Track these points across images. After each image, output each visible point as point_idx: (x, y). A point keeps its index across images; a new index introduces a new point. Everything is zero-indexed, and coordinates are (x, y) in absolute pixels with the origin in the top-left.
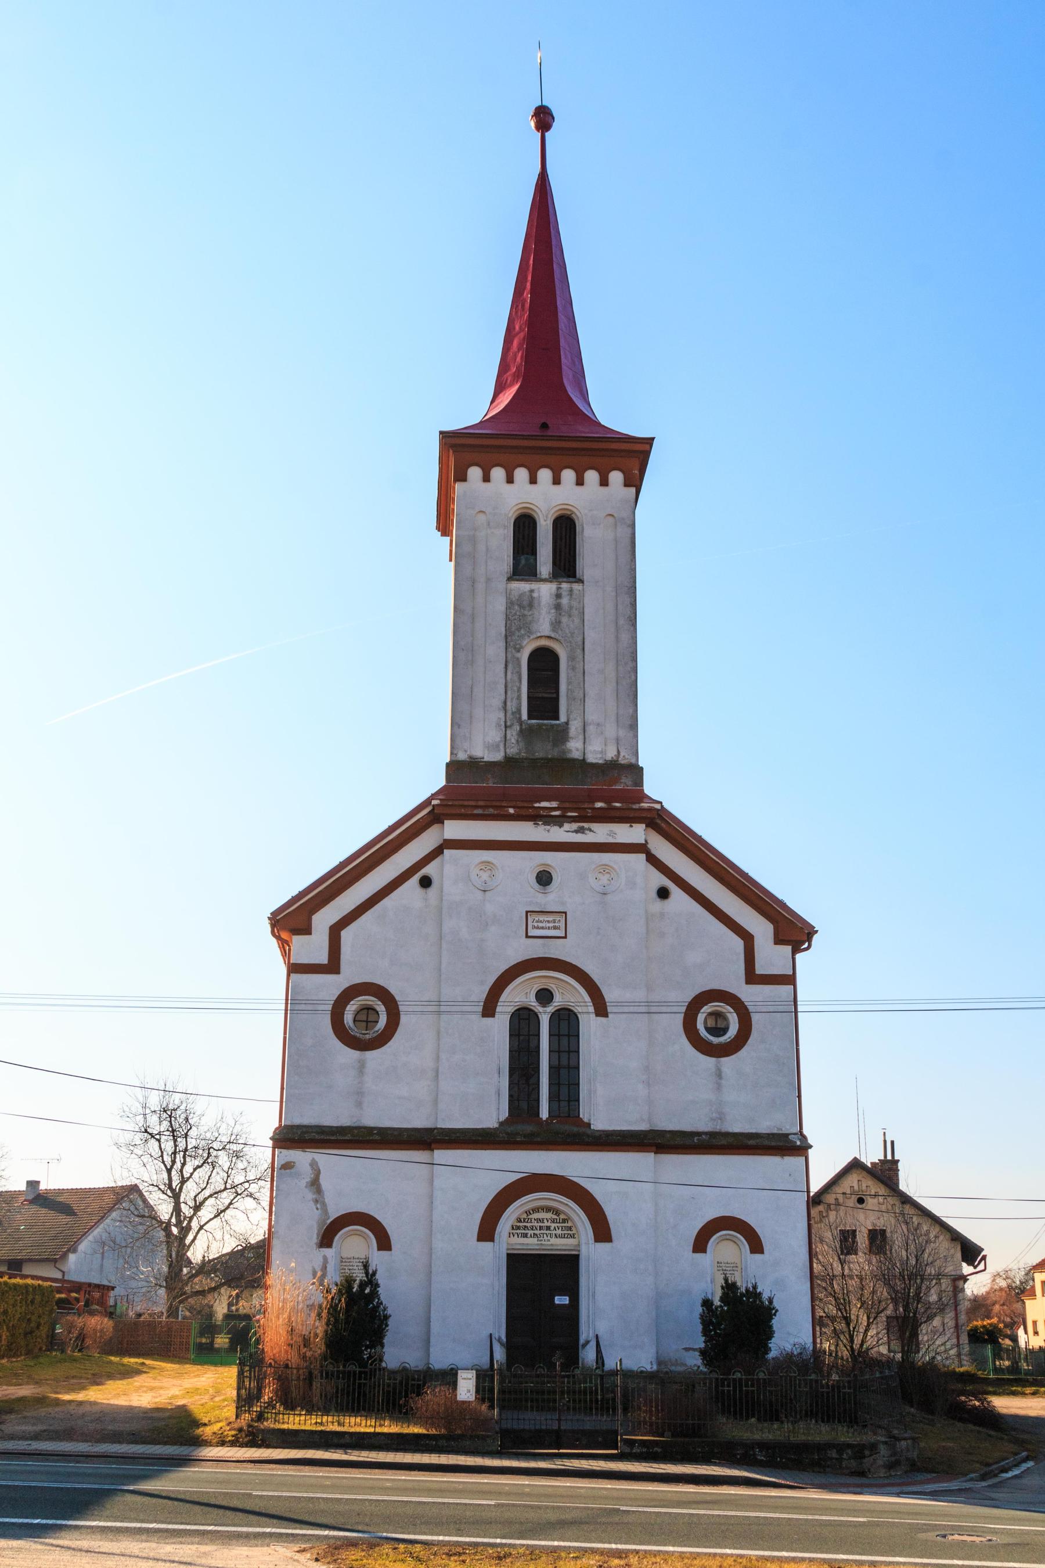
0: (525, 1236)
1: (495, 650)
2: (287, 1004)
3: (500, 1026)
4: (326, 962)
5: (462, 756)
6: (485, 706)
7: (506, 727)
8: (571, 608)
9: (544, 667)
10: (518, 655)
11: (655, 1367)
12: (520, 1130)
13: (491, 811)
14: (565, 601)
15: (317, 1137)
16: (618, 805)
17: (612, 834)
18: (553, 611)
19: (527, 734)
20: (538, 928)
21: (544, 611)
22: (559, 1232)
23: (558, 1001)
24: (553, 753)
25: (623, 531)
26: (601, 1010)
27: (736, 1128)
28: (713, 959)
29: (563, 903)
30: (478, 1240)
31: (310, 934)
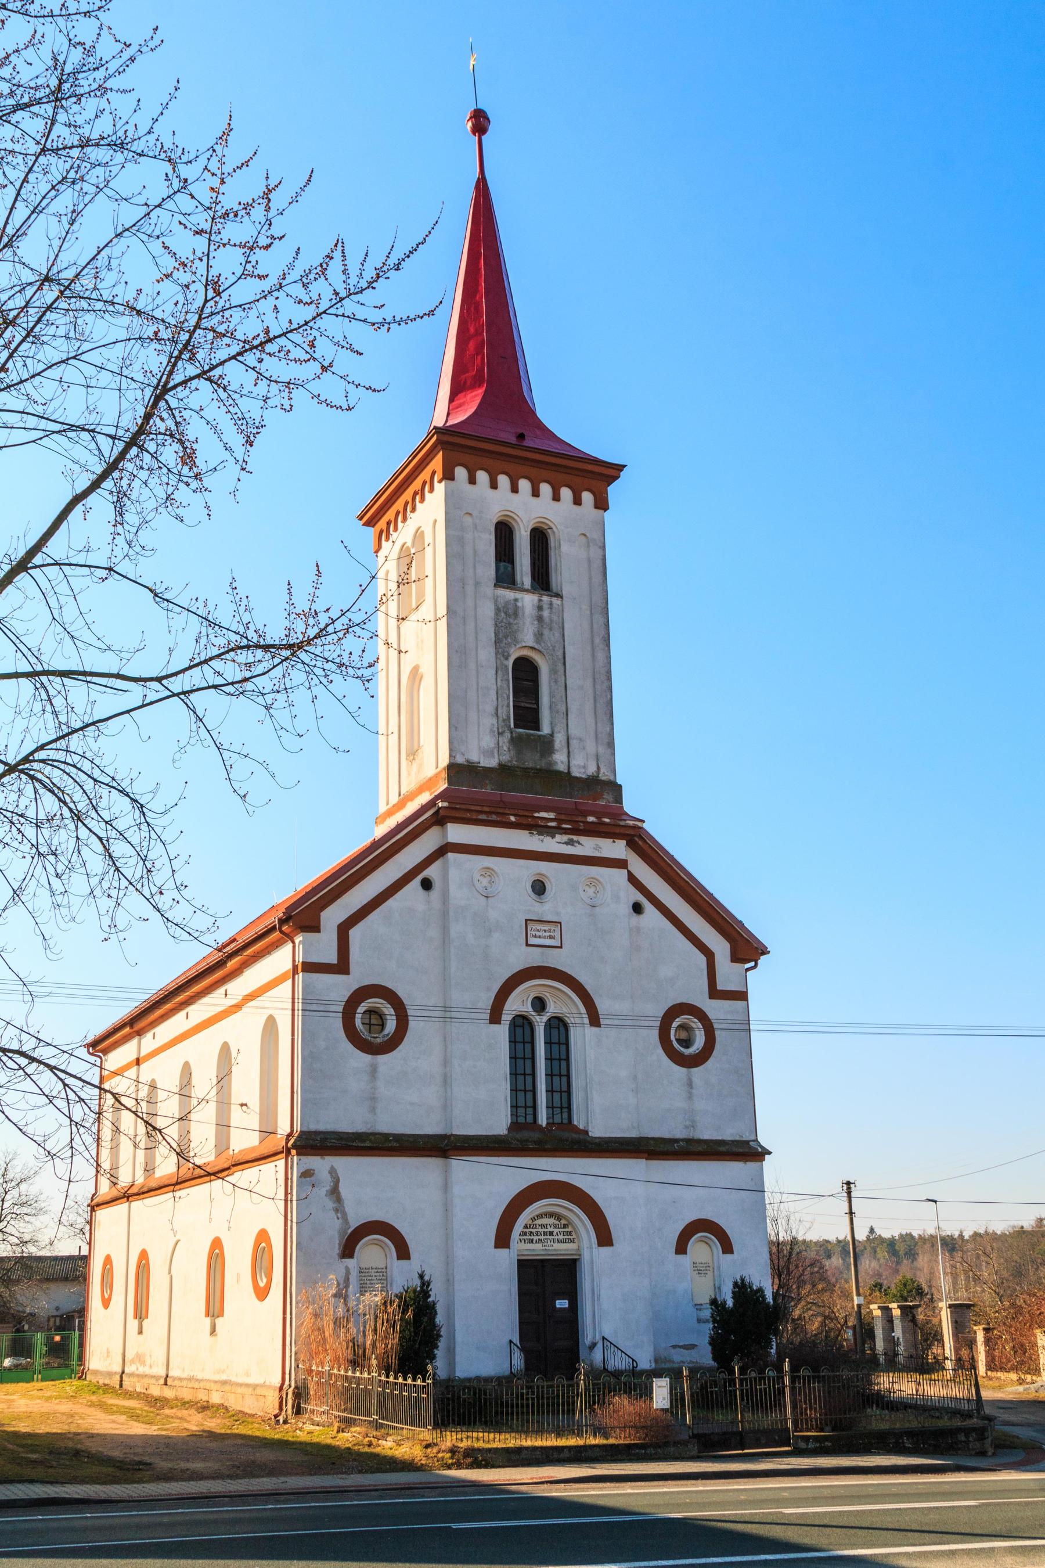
0: (531, 1241)
1: (487, 654)
2: (293, 1002)
3: (502, 1032)
4: (336, 962)
5: (460, 760)
7: (499, 734)
8: (551, 621)
9: (525, 676)
10: (505, 662)
12: (521, 1139)
13: (494, 817)
14: (546, 613)
16: (607, 820)
17: (597, 848)
18: (536, 622)
19: (516, 742)
20: (535, 936)
21: (528, 621)
22: (561, 1237)
23: (553, 1008)
24: (542, 764)
25: (595, 553)
26: (595, 1020)
27: (706, 1136)
28: (681, 975)
29: (558, 914)
30: (496, 1247)
31: (319, 931)
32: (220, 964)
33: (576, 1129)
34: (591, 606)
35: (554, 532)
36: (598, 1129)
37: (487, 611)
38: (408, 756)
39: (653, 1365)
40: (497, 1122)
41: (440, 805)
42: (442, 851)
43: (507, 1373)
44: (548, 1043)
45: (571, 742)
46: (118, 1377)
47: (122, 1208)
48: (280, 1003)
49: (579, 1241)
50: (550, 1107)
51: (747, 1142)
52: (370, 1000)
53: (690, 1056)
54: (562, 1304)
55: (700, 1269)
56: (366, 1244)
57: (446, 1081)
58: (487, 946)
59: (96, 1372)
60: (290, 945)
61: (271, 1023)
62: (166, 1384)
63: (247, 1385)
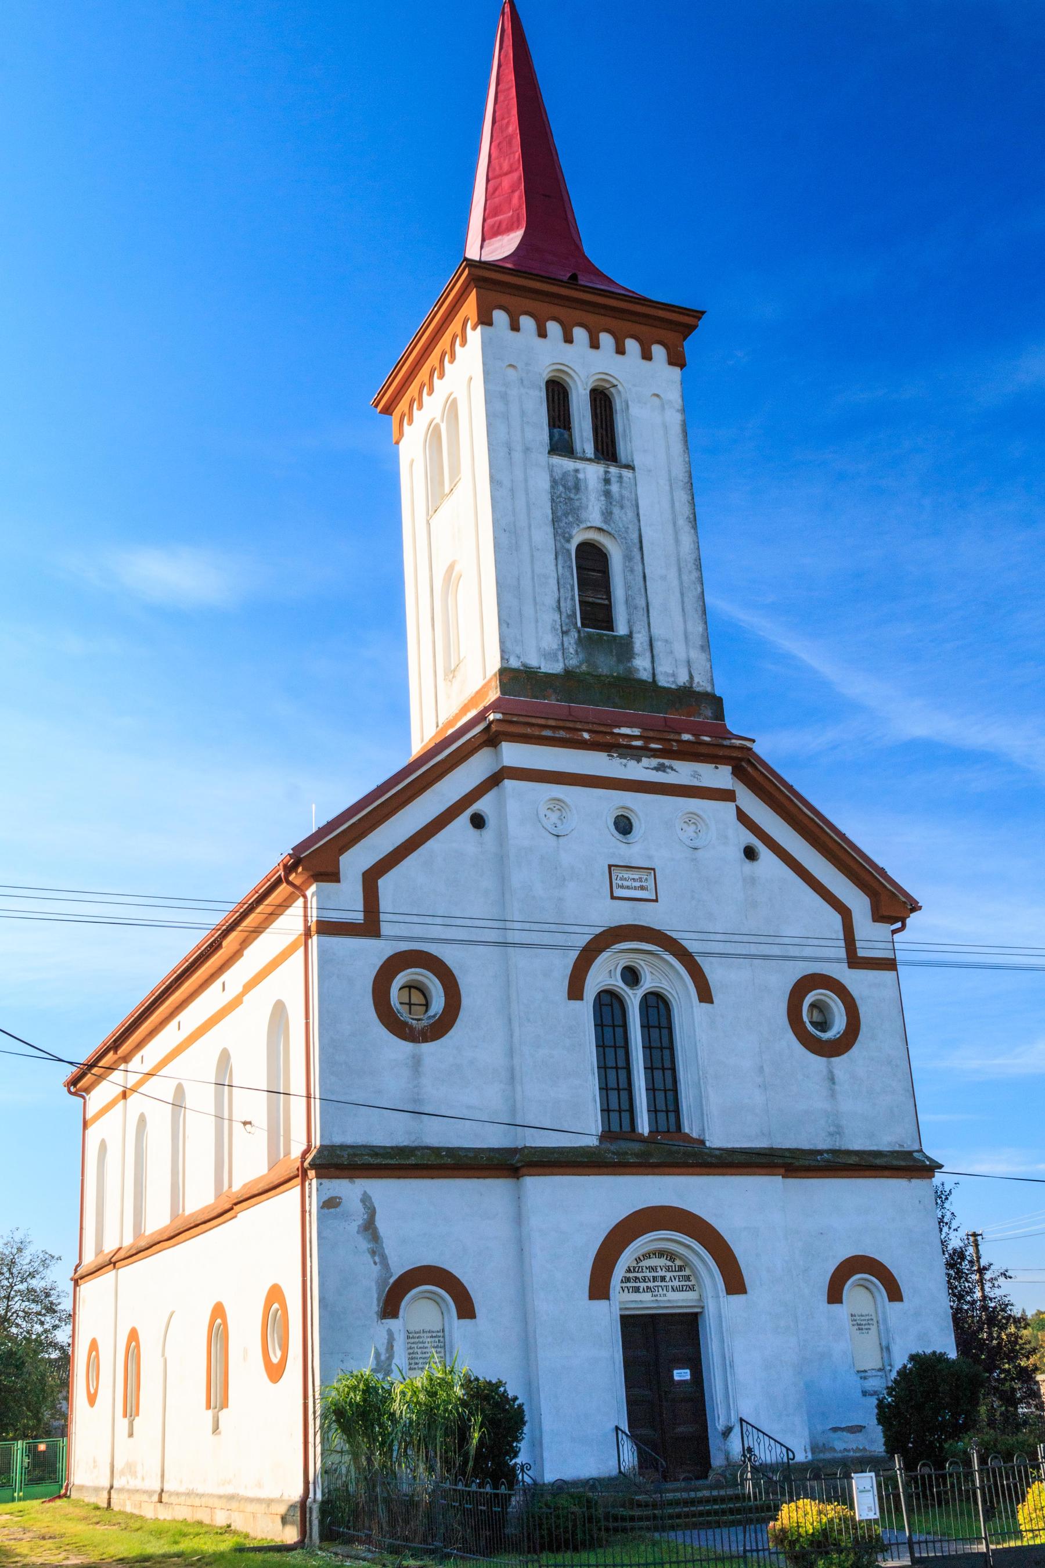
0: (637, 1290)
1: (543, 535)
3: (585, 1009)
5: (514, 663)
6: (535, 604)
7: (563, 633)
8: (622, 497)
9: (591, 565)
10: (567, 546)
11: (810, 1457)
12: (617, 1152)
13: (562, 734)
14: (615, 488)
15: (372, 1161)
17: (696, 775)
18: (603, 498)
20: (622, 887)
22: (676, 1283)
23: (649, 983)
26: (705, 995)
27: (857, 1145)
29: (650, 858)
31: (338, 881)
32: (214, 947)
33: (687, 1137)
34: (670, 480)
35: (619, 392)
36: (717, 1139)
37: (541, 483)
38: (446, 675)
39: (810, 1457)
40: (586, 1128)
41: (491, 717)
42: (494, 780)
43: (615, 1472)
44: (646, 1026)
45: (655, 644)
46: (105, 1495)
47: (107, 1278)
48: (290, 984)
49: (700, 1286)
50: (653, 1110)
51: (910, 1153)
52: (409, 971)
53: (829, 1042)
54: (682, 1375)
55: (860, 1324)
56: (415, 1299)
57: (512, 1078)
58: (560, 899)
59: (81, 1488)
60: (301, 900)
61: (279, 1010)
62: (161, 1502)
63: (259, 1501)
